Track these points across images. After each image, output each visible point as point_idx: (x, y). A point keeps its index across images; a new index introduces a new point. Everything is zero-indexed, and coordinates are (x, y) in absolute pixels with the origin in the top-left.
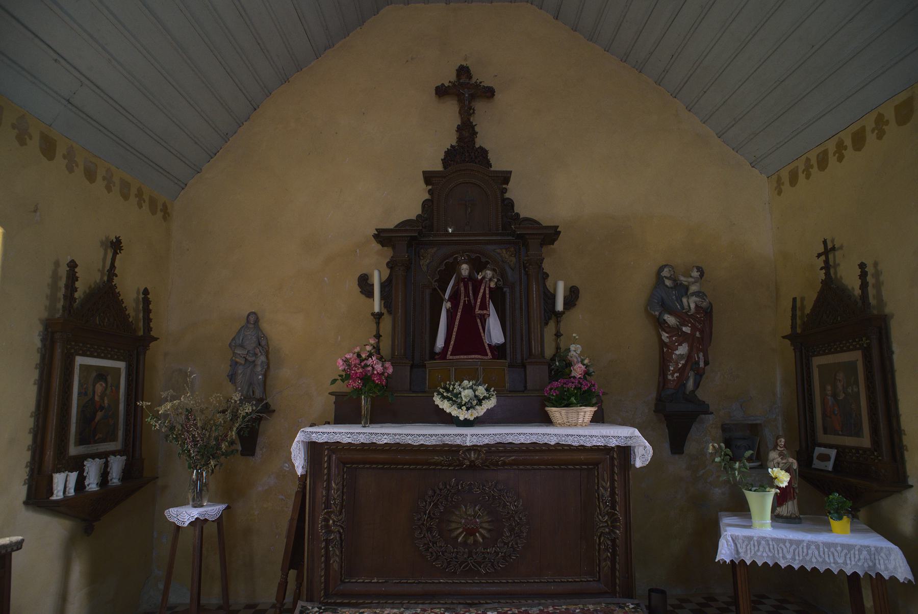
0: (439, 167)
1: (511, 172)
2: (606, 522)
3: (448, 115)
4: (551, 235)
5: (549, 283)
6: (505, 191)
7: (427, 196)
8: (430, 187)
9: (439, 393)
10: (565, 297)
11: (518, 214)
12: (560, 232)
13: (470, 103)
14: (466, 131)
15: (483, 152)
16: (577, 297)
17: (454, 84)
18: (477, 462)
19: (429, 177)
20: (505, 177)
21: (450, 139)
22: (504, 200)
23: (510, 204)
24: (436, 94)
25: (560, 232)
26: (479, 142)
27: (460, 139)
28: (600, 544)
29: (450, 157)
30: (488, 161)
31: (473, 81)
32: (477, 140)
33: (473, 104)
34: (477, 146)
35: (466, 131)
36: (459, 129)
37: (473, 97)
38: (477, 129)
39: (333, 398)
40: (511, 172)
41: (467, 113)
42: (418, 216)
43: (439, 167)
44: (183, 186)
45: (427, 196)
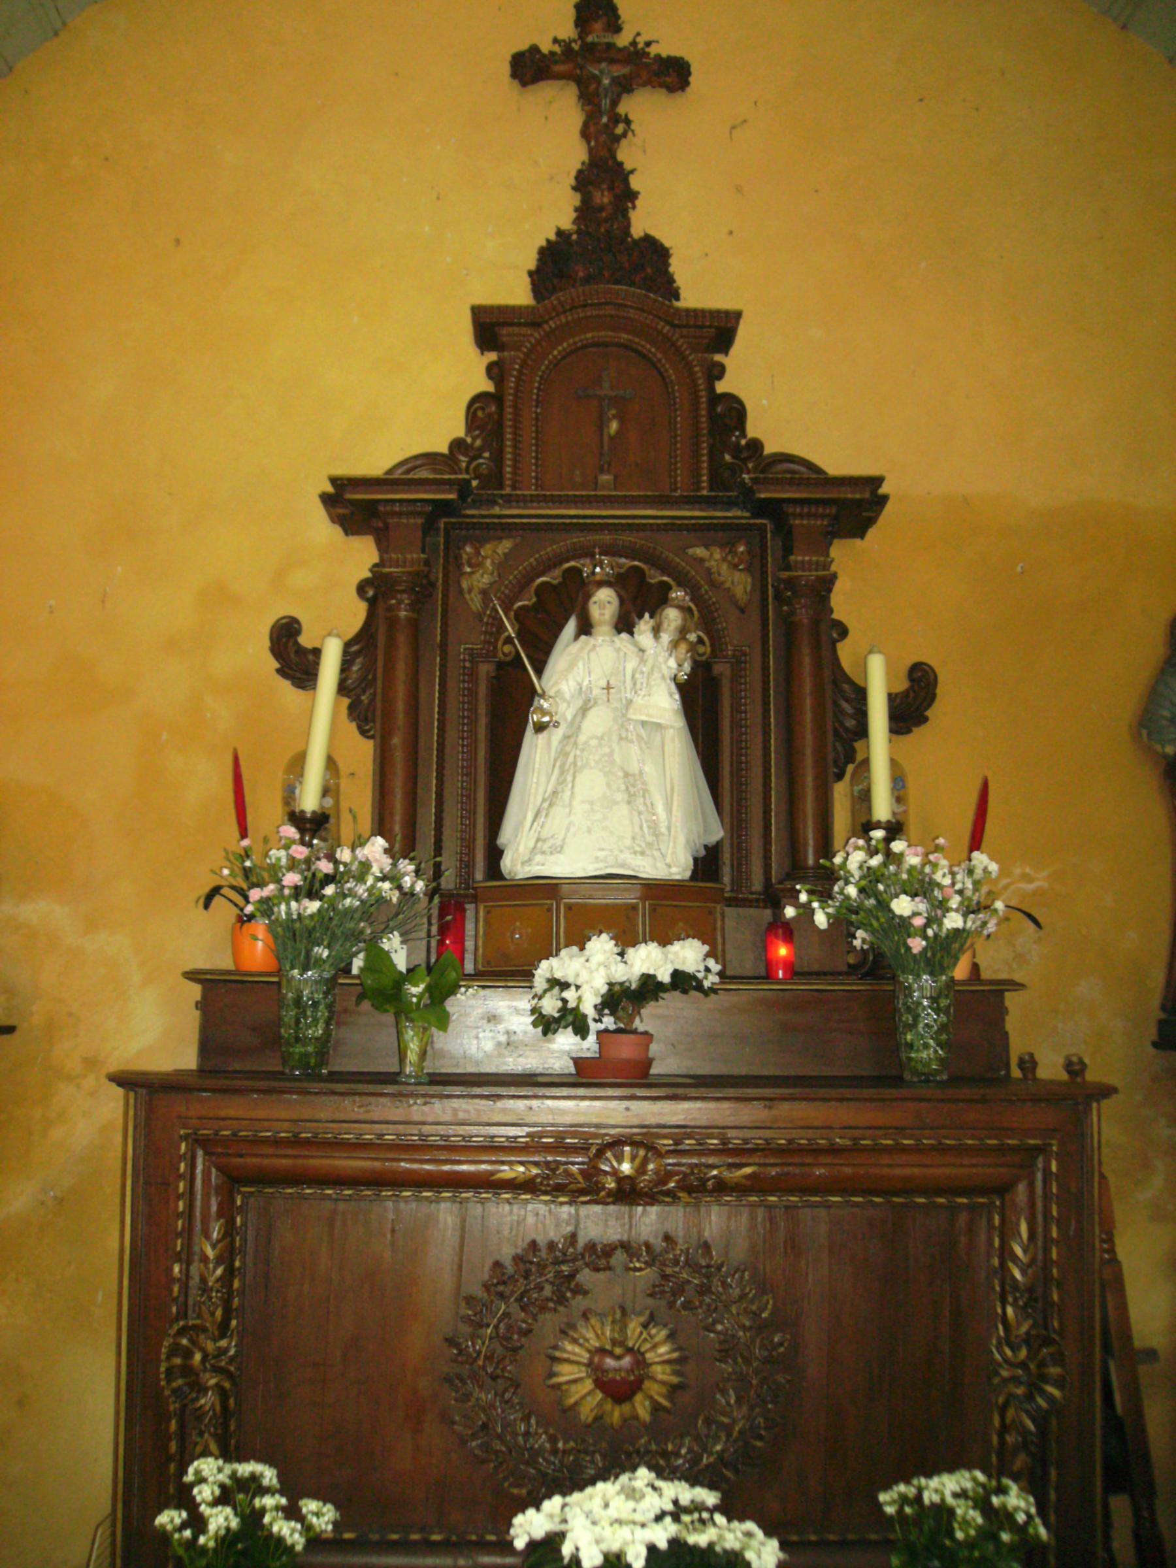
0: (519, 294)
1: (738, 315)
2: (1023, 1365)
3: (553, 129)
4: (856, 505)
5: (845, 652)
6: (719, 372)
7: (486, 385)
8: (493, 356)
9: (794, 515)
10: (891, 698)
11: (756, 445)
12: (885, 499)
13: (615, 103)
14: (604, 183)
15: (654, 253)
16: (930, 698)
17: (566, 46)
18: (643, 1182)
19: (489, 327)
20: (721, 330)
21: (559, 212)
22: (716, 399)
23: (732, 412)
24: (514, 75)
25: (885, 499)
26: (641, 223)
27: (585, 212)
28: (1004, 1429)
29: (554, 264)
30: (671, 280)
31: (623, 40)
32: (634, 216)
33: (622, 109)
34: (637, 231)
35: (604, 183)
36: (583, 182)
37: (625, 86)
38: (635, 183)
39: (195, 991)
40: (738, 315)
41: (604, 133)
42: (457, 445)
43: (519, 294)
44: (58, 24)
45: (486, 385)
